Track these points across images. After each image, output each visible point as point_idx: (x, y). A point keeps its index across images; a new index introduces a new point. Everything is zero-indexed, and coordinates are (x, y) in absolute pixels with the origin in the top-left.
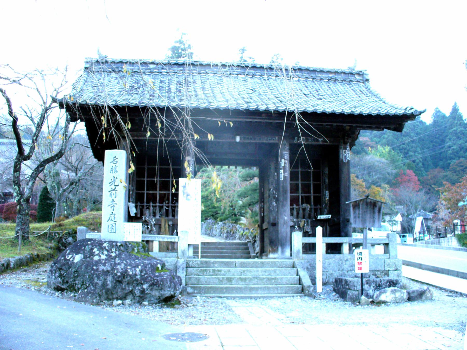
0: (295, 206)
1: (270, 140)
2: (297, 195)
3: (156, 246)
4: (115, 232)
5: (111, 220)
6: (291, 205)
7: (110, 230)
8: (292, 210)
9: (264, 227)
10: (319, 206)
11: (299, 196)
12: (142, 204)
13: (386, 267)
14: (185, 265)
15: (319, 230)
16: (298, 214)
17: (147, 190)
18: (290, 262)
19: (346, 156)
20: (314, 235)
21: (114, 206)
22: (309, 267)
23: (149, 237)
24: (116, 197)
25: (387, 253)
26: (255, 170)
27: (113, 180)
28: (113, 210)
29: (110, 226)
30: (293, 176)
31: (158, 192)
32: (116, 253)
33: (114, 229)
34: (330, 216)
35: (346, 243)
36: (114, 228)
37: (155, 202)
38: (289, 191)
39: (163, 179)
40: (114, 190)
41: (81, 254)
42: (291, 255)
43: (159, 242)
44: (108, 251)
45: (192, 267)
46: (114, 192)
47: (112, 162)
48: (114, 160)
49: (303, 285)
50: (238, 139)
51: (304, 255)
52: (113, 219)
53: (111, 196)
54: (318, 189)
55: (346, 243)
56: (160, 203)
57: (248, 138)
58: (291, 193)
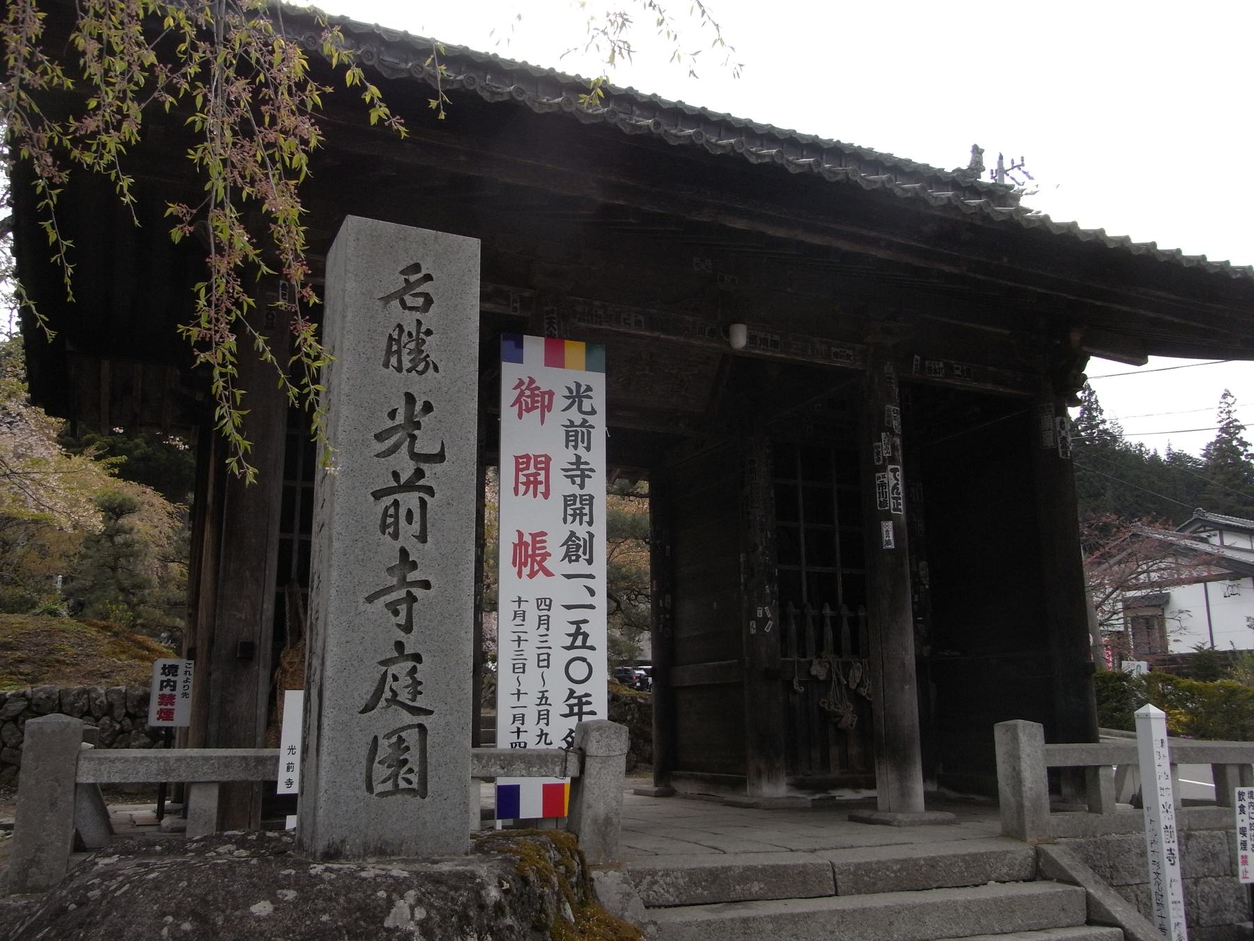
4: (422, 791)
5: (394, 700)
7: (380, 771)
21: (411, 599)
24: (422, 538)
27: (400, 418)
28: (408, 628)
33: (413, 757)
36: (413, 757)
40: (409, 487)
46: (410, 500)
52: (404, 697)
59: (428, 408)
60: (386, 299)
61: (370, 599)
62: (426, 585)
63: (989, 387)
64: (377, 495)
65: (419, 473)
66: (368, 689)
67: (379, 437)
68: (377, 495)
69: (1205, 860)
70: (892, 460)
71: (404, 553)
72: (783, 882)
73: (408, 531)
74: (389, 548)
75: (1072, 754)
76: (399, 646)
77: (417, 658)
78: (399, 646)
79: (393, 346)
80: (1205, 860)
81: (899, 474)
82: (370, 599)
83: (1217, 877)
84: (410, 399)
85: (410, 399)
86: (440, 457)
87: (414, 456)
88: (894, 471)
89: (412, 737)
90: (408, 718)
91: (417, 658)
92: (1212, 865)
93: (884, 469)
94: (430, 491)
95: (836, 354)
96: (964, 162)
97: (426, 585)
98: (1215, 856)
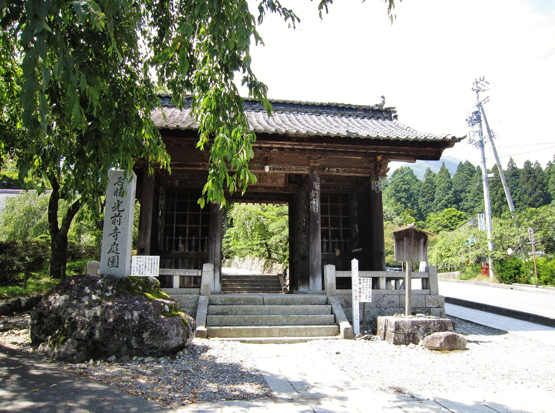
0: (325, 240)
1: (300, 170)
2: (327, 228)
3: (176, 281)
4: (118, 267)
5: (113, 252)
6: (322, 238)
7: (110, 263)
8: (322, 243)
9: (295, 261)
10: (348, 240)
11: (328, 230)
12: (343, 274)
13: (427, 304)
14: (207, 302)
15: (355, 263)
16: (328, 248)
17: (176, 224)
18: (323, 298)
19: (378, 187)
20: (349, 268)
21: (117, 235)
22: (344, 304)
23: (168, 272)
24: (119, 224)
25: (427, 288)
26: (286, 208)
27: (116, 204)
28: (116, 240)
29: (111, 260)
30: (323, 209)
31: (187, 226)
32: (112, 292)
33: (116, 261)
34: (360, 249)
35: (383, 277)
36: (116, 261)
37: (184, 236)
38: (320, 226)
39: (193, 213)
40: (118, 216)
41: (67, 294)
42: (323, 288)
43: (181, 276)
44: (102, 289)
45: (215, 305)
46: (118, 218)
47: (117, 183)
48: (119, 181)
49: (335, 315)
50: (267, 169)
51: (338, 291)
52: (115, 251)
53: (113, 223)
54: (346, 223)
55: (383, 277)
56: (189, 237)
57: (277, 169)
58: (321, 227)
59: (122, 202)
60: (115, 184)
61: (110, 235)
62: (120, 232)
63: (352, 174)
64: (112, 218)
65: (120, 214)
66: (109, 250)
67: (113, 208)
68: (112, 218)
69: (390, 303)
70: (315, 197)
71: (116, 227)
72: (248, 302)
73: (117, 223)
74: (113, 227)
75: (343, 274)
76: (115, 243)
77: (118, 245)
78: (115, 243)
79: (116, 192)
80: (390, 303)
81: (317, 201)
82: (110, 235)
83: (394, 308)
84: (118, 201)
85: (118, 201)
86: (123, 211)
87: (119, 211)
88: (315, 200)
89: (116, 258)
90: (115, 254)
91: (118, 245)
92: (392, 304)
93: (312, 200)
94: (121, 217)
95: (300, 170)
96: (379, 102)
97: (120, 232)
98: (393, 302)
